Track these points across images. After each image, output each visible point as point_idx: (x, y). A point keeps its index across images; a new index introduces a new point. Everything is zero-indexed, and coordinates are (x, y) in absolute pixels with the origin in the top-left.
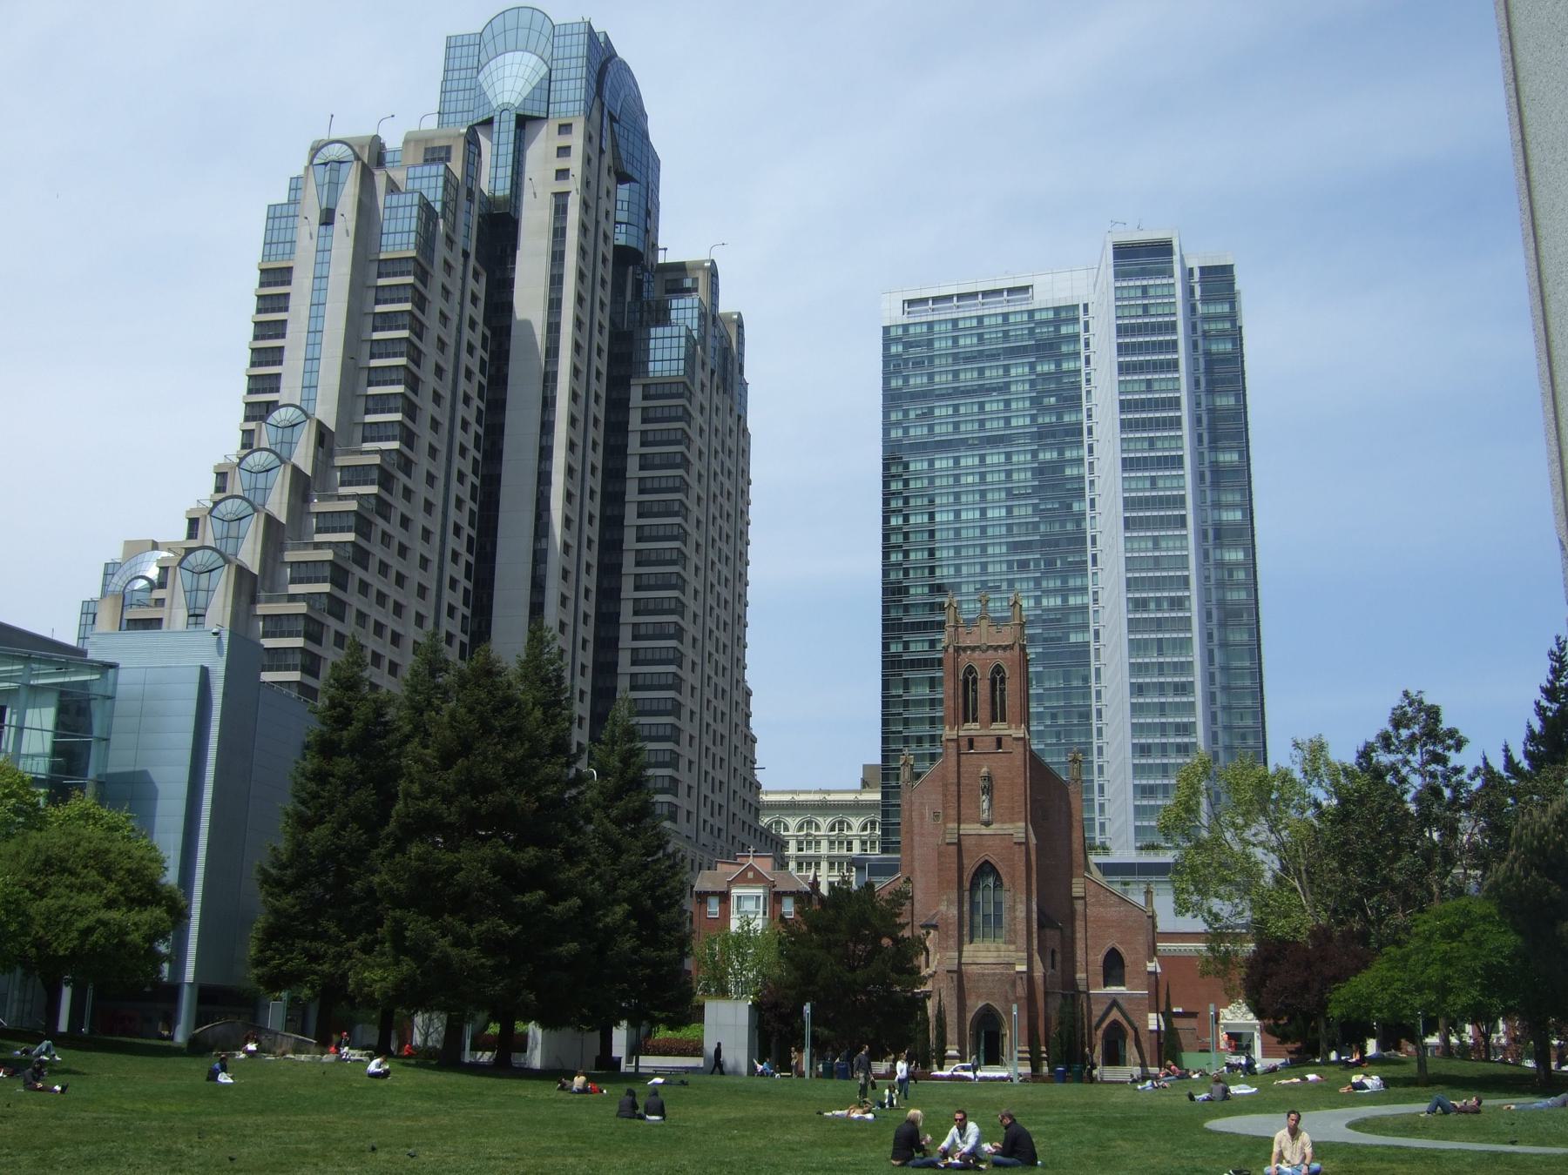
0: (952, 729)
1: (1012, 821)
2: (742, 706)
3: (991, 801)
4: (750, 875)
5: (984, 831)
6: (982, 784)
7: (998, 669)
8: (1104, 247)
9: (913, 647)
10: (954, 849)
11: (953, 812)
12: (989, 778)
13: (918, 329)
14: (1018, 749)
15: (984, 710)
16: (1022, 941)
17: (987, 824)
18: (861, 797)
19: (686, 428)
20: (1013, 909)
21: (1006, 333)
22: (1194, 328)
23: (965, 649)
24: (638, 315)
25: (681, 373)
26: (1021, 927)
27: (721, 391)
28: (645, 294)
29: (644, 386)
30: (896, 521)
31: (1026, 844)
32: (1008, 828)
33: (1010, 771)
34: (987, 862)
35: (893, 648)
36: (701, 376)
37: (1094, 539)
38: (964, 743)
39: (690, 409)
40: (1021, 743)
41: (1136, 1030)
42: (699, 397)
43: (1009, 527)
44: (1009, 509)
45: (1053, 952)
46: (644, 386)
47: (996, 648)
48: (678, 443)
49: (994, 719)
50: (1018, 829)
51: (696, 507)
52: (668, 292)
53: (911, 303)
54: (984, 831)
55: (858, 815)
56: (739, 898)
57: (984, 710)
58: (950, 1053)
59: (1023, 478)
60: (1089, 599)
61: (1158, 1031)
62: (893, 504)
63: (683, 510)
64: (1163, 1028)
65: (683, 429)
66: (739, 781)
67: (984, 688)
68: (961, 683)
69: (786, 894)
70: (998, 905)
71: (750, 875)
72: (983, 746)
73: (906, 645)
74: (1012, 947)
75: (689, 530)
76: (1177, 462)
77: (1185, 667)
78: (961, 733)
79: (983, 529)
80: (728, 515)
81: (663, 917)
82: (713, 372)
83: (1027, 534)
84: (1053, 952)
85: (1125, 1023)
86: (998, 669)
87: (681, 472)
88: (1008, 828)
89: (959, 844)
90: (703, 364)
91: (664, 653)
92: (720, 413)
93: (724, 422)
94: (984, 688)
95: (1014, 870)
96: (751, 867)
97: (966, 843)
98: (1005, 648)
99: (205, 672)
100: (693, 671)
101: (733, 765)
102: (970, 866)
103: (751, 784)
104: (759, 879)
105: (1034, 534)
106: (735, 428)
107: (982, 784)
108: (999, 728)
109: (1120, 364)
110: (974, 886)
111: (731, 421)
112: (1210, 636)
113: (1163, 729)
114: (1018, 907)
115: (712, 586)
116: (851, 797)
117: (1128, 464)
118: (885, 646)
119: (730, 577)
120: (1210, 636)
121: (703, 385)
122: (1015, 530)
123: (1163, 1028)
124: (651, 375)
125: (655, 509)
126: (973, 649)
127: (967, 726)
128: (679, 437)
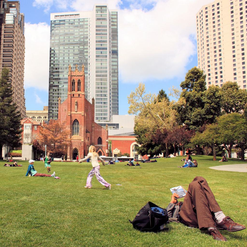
0: (69, 92)
1: (81, 111)
2: (23, 92)
3: (77, 107)
4: (28, 121)
5: (76, 113)
6: (76, 103)
7: (79, 80)
8: (94, 6)
9: (55, 83)
10: (69, 117)
11: (70, 109)
12: (77, 102)
13: (57, 21)
14: (83, 96)
15: (76, 88)
16: (83, 135)
17: (76, 112)
18: (43, 112)
19: (13, 49)
20: (81, 129)
21: (64, 40)
22: (110, 24)
23: (73, 76)
24: (3, 11)
25: (12, 23)
26: (83, 133)
27: (20, 28)
28: (5, 7)
29: (5, 25)
30: (52, 62)
31: (84, 116)
32: (80, 113)
33: (81, 101)
34: (76, 119)
35: (51, 83)
36: (16, 24)
37: (89, 63)
38: (72, 95)
39: (14, 40)
40: (84, 95)
41: (104, 153)
42: (16, 29)
43: (74, 61)
44: (74, 57)
45: (88, 138)
46: (5, 25)
47: (79, 76)
48: (10, 62)
49: (78, 91)
50: (82, 113)
51: (15, 42)
52: (10, 7)
53: (56, 16)
54: (76, 113)
55: (42, 116)
56: (26, 126)
57: (76, 88)
58: (68, 157)
59: (77, 51)
60: (88, 23)
61: (108, 153)
62: (52, 56)
63: (13, 32)
64: (109, 152)
65: (12, 44)
66: (22, 107)
67: (76, 84)
68: (72, 83)
69: (35, 125)
70: (78, 128)
71: (28, 121)
72: (76, 96)
73: (54, 82)
74: (81, 136)
75: (13, 55)
76: (106, 49)
77: (105, 88)
78: (72, 93)
79: (69, 61)
80: (21, 58)
81: (12, 104)
82: (18, 24)
83: (77, 62)
84: (88, 138)
85: (102, 151)
86: (79, 80)
87: (11, 63)
88: (80, 113)
89: (71, 116)
90: (17, 22)
91: (9, 60)
92: (20, 33)
93: (20, 35)
94: (76, 84)
95: (81, 121)
96: (28, 120)
97: (72, 115)
98: (81, 76)
99: (20, 156)
100: (14, 84)
101: (21, 108)
102: (73, 120)
103: (24, 107)
104: (30, 122)
105: (78, 62)
106: (22, 37)
107: (76, 103)
108: (79, 92)
109: (96, 30)
110: (73, 124)
111: (22, 35)
112: (110, 82)
113: (101, 111)
114: (82, 128)
115: (17, 77)
116: (41, 112)
117: (97, 49)
118: (50, 83)
119: (21, 66)
120: (110, 82)
121: (16, 26)
122: (75, 61)
123: (109, 152)
124: (6, 23)
125: (7, 51)
126: (74, 76)
127: (73, 92)
128: (11, 61)
